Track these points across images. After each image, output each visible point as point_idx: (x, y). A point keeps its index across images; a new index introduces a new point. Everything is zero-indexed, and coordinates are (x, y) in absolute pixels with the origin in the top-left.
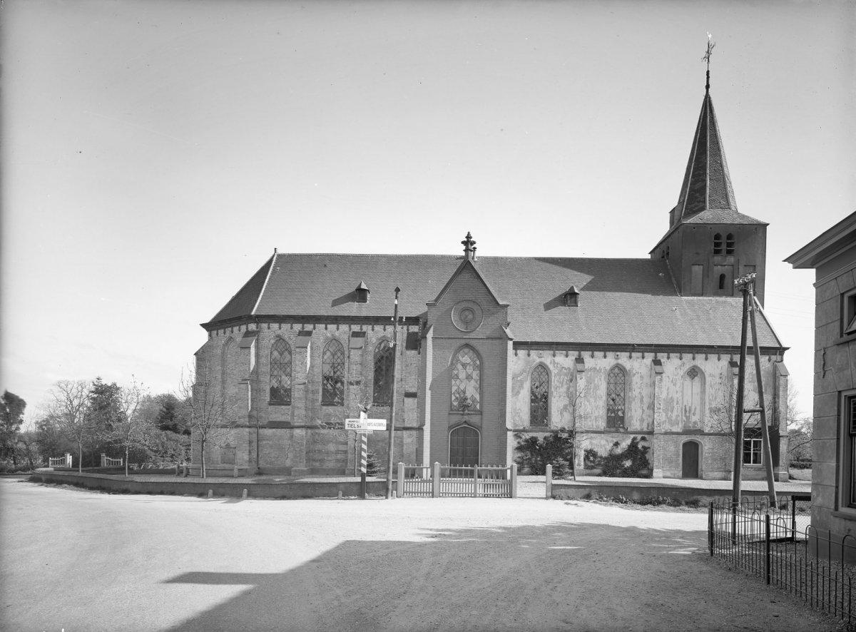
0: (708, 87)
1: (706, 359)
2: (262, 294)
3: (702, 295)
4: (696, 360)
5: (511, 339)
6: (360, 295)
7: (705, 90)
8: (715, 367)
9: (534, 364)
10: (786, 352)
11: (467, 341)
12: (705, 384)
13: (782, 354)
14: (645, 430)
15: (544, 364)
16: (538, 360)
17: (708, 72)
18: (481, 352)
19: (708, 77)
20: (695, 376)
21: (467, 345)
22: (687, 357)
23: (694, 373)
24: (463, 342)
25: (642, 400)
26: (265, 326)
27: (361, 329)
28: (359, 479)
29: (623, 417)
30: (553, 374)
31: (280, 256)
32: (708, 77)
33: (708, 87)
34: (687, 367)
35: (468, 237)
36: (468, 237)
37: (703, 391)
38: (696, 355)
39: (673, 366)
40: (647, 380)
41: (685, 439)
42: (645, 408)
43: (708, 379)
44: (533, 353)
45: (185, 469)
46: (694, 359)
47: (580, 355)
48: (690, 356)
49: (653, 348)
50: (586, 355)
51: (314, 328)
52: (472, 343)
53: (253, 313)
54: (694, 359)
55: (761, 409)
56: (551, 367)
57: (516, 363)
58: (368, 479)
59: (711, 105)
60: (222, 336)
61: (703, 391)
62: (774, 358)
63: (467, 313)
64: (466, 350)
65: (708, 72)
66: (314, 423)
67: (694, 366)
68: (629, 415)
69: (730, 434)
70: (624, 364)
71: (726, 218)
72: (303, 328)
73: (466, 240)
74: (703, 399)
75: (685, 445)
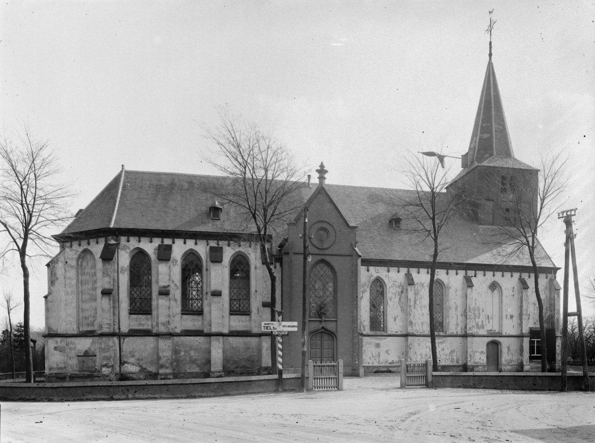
0: (490, 55)
1: (503, 276)
2: (116, 209)
3: (493, 224)
4: (495, 277)
5: (360, 256)
6: (215, 211)
7: (488, 58)
8: (509, 282)
9: (372, 279)
10: (558, 271)
11: (323, 257)
12: (502, 295)
13: (555, 273)
14: (459, 333)
15: (380, 278)
16: (375, 275)
17: (490, 43)
18: (337, 269)
19: (491, 47)
20: (494, 290)
21: (323, 261)
22: (489, 274)
23: (494, 286)
24: (319, 258)
25: (456, 309)
26: (123, 239)
27: (218, 244)
28: (276, 376)
29: (442, 323)
30: (388, 287)
31: (126, 172)
32: (491, 47)
33: (490, 55)
34: (489, 282)
35: (322, 166)
36: (322, 166)
37: (501, 302)
38: (496, 273)
39: (481, 281)
40: (460, 293)
41: (490, 339)
42: (459, 315)
43: (505, 292)
44: (372, 268)
45: (43, 371)
46: (494, 275)
47: (408, 272)
48: (491, 273)
49: (464, 266)
50: (413, 271)
51: (174, 243)
52: (328, 258)
53: (112, 226)
54: (494, 275)
55: (578, 313)
56: (386, 281)
57: (366, 275)
58: (284, 376)
59: (493, 72)
60: (77, 248)
61: (501, 302)
62: (550, 276)
63: (322, 232)
64: (322, 265)
65: (490, 43)
66: (490, 319)
67: (494, 282)
68: (447, 321)
69: (466, 332)
70: (443, 280)
71: (509, 164)
72: (162, 242)
73: (319, 168)
74: (501, 308)
75: (488, 344)
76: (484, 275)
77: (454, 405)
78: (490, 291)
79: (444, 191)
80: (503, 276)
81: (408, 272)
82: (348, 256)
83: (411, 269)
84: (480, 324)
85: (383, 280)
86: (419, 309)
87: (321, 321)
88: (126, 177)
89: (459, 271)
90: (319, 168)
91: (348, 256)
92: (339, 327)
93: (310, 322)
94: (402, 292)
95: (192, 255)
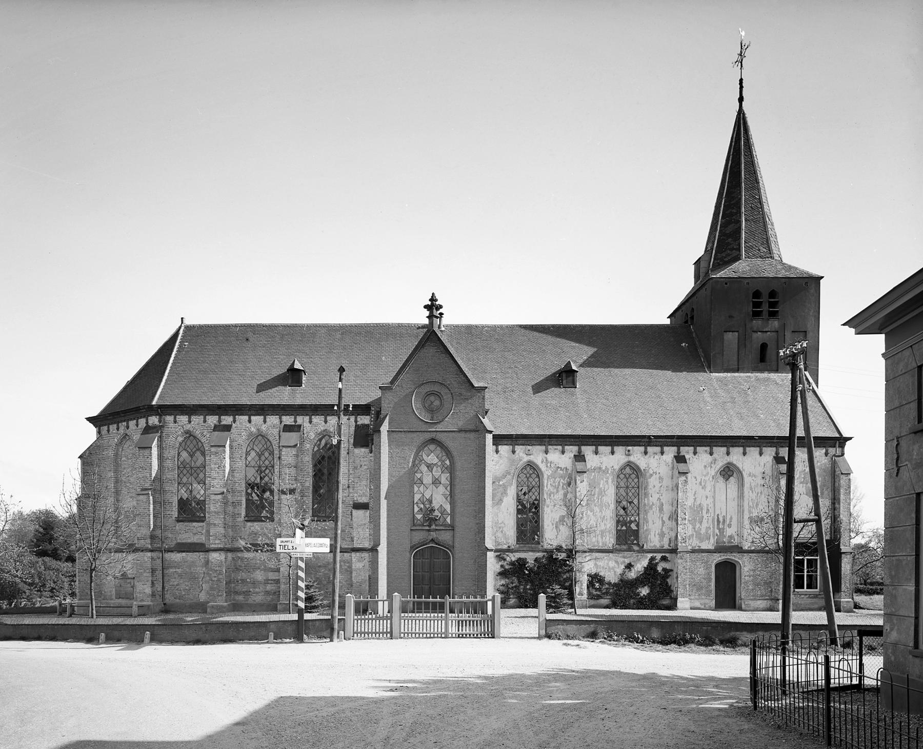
0: (741, 99)
1: (744, 454)
5: (491, 432)
13: (842, 446)
16: (526, 459)
17: (741, 80)
19: (741, 87)
20: (730, 476)
21: (433, 441)
22: (720, 451)
23: (728, 472)
24: (428, 436)
27: (295, 421)
28: (295, 617)
29: (637, 531)
30: (545, 476)
32: (741, 87)
33: (741, 99)
34: (720, 464)
35: (433, 299)
36: (433, 299)
37: (741, 496)
38: (731, 449)
39: (701, 463)
40: (667, 482)
43: (747, 480)
46: (728, 454)
48: (724, 449)
49: (675, 440)
51: (234, 421)
52: (440, 437)
56: (543, 467)
57: (498, 462)
58: (307, 616)
59: (745, 123)
60: (115, 432)
61: (741, 496)
62: (832, 451)
64: (432, 447)
65: (741, 80)
67: (729, 463)
68: (645, 528)
70: (638, 463)
71: (767, 270)
72: (220, 421)
73: (429, 303)
74: (740, 507)
76: (711, 454)
77: (371, 682)
78: (721, 480)
79: (668, 322)
80: (744, 454)
81: (580, 451)
82: (470, 431)
83: (583, 448)
84: (703, 531)
85: (537, 466)
86: (596, 509)
87: (429, 530)
88: (185, 332)
89: (666, 448)
90: (429, 303)
91: (470, 431)
92: (457, 540)
93: (414, 533)
94: (569, 484)
95: (260, 438)
